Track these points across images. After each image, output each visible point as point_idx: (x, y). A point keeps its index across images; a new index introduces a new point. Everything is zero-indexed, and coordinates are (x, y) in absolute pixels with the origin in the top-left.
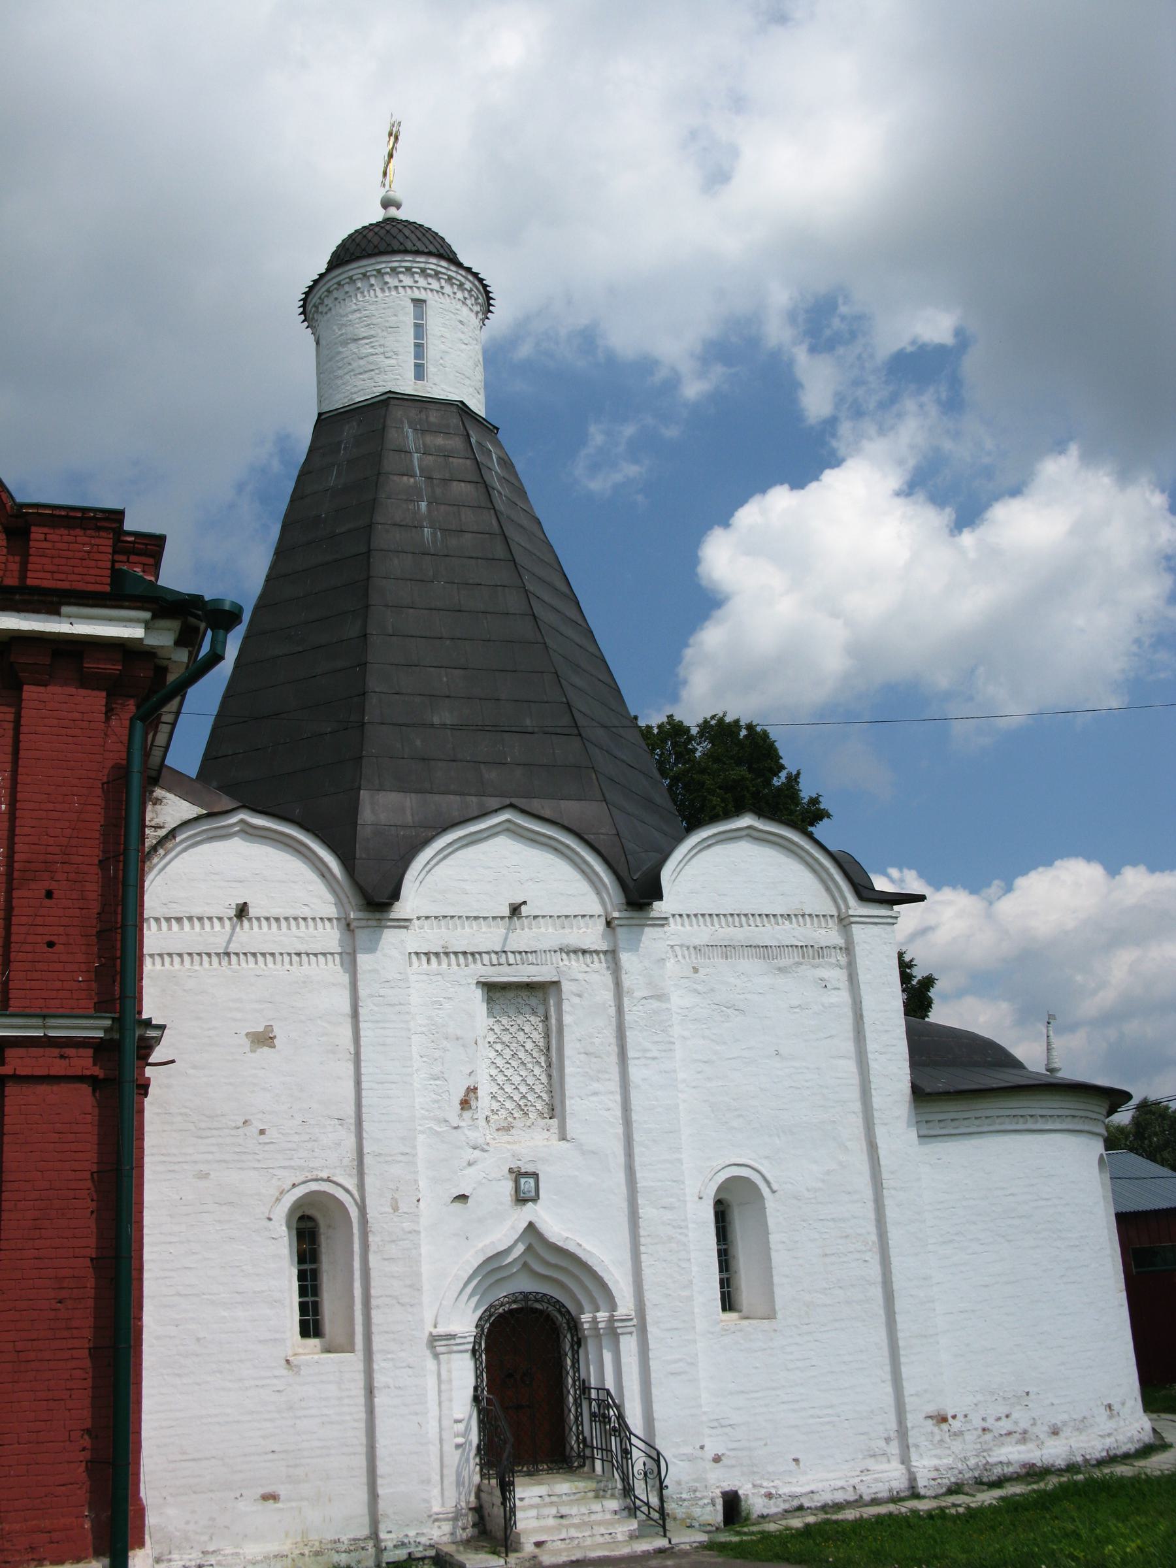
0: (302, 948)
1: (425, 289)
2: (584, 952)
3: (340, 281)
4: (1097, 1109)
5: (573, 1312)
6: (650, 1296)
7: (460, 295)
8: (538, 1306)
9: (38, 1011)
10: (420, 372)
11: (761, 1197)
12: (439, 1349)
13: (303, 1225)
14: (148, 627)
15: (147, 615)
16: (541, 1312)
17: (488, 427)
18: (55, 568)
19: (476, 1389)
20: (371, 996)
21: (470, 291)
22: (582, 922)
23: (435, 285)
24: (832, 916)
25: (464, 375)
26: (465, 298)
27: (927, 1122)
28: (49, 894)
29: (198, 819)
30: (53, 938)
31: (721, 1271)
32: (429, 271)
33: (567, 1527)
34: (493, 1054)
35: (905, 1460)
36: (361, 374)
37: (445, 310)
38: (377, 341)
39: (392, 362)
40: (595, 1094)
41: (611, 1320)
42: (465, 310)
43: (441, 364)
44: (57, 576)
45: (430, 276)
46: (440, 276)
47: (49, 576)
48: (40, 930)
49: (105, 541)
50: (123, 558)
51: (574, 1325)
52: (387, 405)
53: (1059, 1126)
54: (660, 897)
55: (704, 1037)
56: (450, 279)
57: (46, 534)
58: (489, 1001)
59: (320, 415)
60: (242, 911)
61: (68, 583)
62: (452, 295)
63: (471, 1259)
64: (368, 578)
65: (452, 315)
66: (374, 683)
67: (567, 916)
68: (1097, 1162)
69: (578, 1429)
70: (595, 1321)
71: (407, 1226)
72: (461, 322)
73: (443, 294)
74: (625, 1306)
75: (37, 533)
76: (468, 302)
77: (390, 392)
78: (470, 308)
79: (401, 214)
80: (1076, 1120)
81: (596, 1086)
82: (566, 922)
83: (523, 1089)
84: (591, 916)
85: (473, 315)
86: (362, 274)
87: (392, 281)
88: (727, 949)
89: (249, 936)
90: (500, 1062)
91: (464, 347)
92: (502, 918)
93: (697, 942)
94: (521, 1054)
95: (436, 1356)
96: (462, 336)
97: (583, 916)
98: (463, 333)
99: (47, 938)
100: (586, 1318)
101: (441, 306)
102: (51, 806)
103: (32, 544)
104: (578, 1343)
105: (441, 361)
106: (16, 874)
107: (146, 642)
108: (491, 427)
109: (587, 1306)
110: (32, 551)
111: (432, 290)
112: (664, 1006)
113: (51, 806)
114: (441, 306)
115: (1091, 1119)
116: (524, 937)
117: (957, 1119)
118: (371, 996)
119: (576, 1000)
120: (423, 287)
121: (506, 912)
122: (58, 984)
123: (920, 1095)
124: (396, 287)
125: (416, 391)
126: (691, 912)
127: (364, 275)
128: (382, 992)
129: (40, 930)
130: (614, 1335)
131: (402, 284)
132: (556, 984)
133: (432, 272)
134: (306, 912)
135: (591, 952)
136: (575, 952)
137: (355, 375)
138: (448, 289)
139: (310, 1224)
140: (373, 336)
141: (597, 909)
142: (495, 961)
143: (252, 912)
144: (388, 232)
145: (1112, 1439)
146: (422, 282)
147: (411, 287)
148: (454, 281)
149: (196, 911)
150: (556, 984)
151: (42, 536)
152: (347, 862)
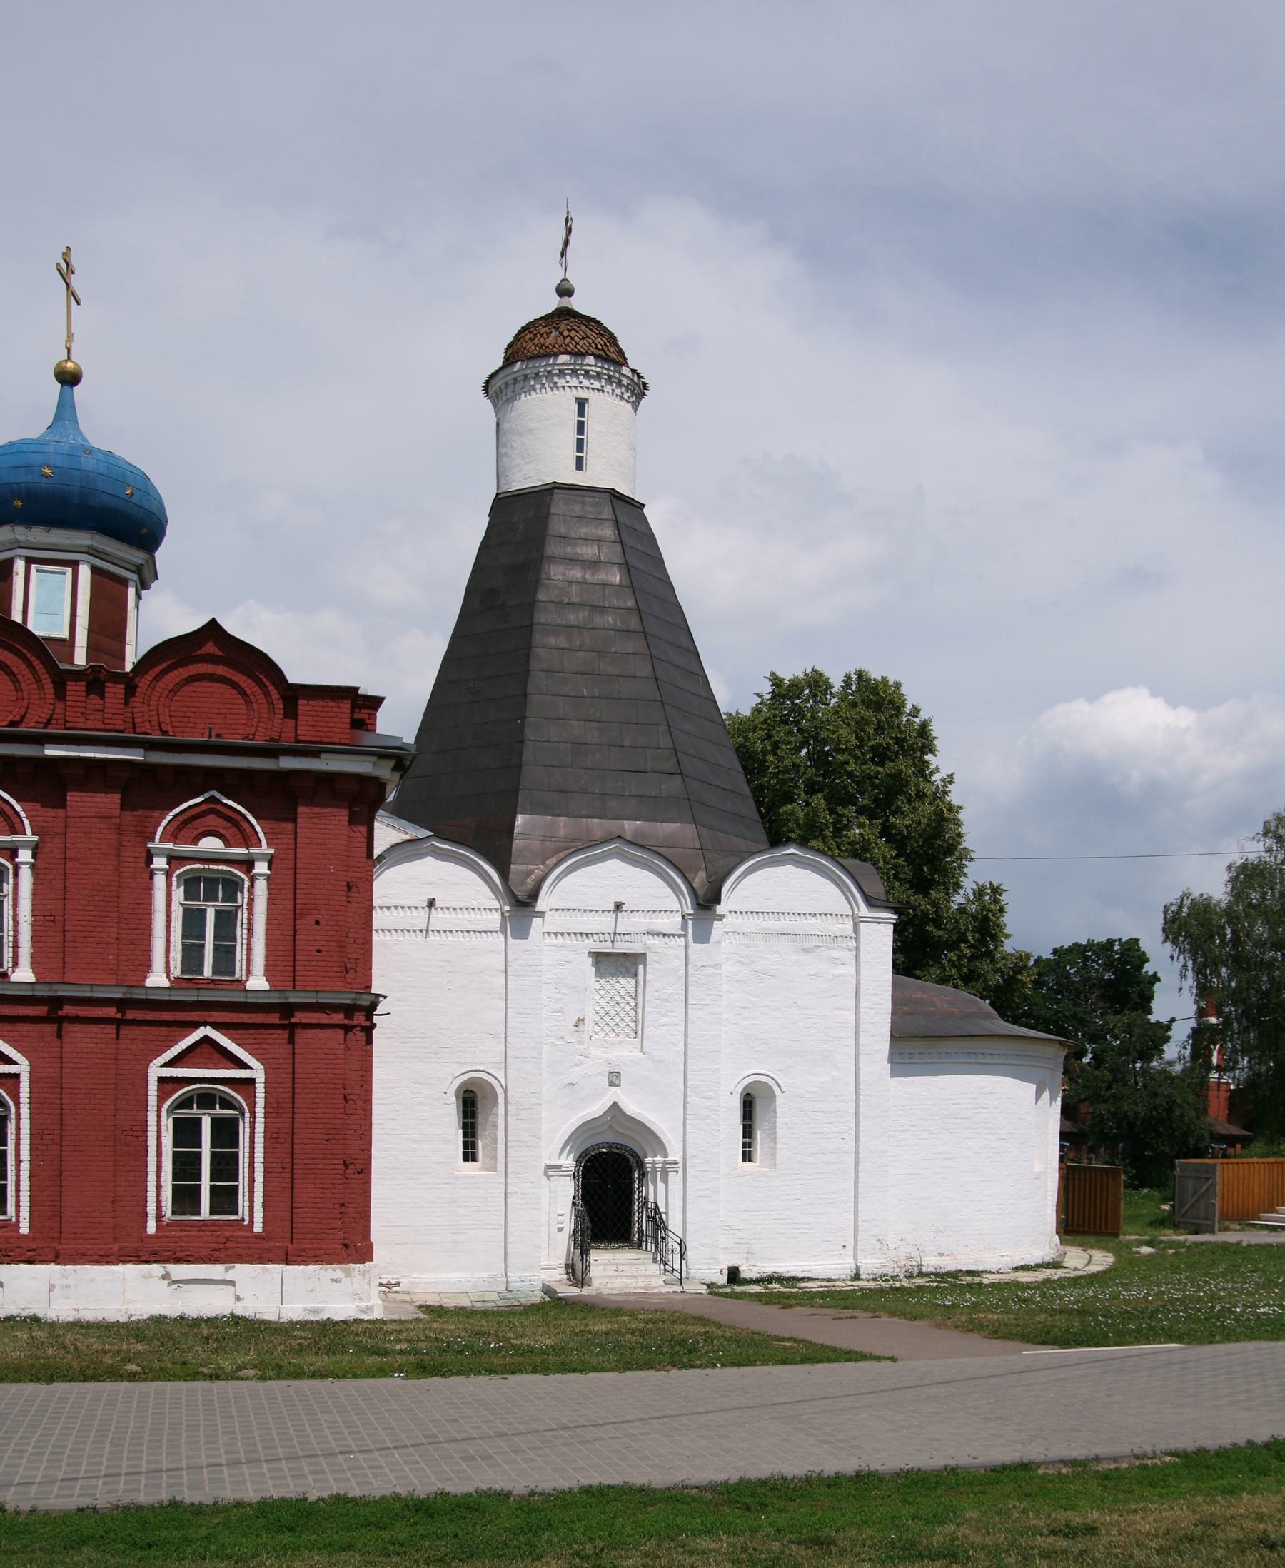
0: (471, 928)
1: (588, 388)
2: (664, 935)
5: (641, 1156)
6: (690, 1152)
7: (618, 391)
8: (618, 1151)
9: (312, 989)
10: (580, 464)
11: (773, 1096)
12: (550, 1173)
13: (467, 1095)
16: (620, 1155)
18: (314, 723)
19: (574, 1198)
20: (516, 960)
22: (665, 915)
23: (597, 385)
24: (847, 916)
28: (317, 923)
30: (321, 948)
31: (744, 1137)
33: (622, 1276)
34: (597, 997)
35: (855, 1258)
41: (665, 1163)
44: (316, 729)
45: (593, 377)
47: (310, 728)
48: (312, 943)
49: (346, 705)
50: (357, 711)
51: (641, 1165)
52: (552, 494)
54: (719, 903)
55: (744, 992)
56: (610, 377)
59: (497, 494)
60: (431, 903)
63: (574, 1122)
64: (530, 648)
66: (529, 733)
67: (654, 911)
70: (654, 1163)
71: (533, 1100)
74: (675, 1155)
76: (626, 396)
81: (666, 1020)
82: (653, 915)
83: (617, 1020)
84: (671, 911)
87: (561, 382)
88: (768, 934)
89: (439, 919)
90: (602, 1002)
92: (609, 911)
93: (746, 930)
94: (618, 998)
95: (548, 1178)
97: (666, 911)
99: (316, 948)
100: (648, 1160)
102: (316, 871)
103: (299, 708)
104: (643, 1175)
106: (298, 911)
109: (649, 1154)
110: (300, 712)
111: (593, 389)
112: (718, 972)
113: (316, 871)
116: (626, 922)
118: (516, 960)
119: (657, 965)
121: (612, 907)
122: (323, 974)
123: (898, 1037)
124: (563, 387)
126: (744, 910)
127: (537, 374)
128: (523, 957)
129: (312, 943)
130: (665, 1173)
132: (644, 955)
134: (474, 904)
135: (669, 935)
136: (658, 934)
139: (471, 1095)
141: (677, 906)
142: (602, 939)
143: (438, 904)
145: (1009, 1259)
146: (586, 383)
147: (576, 387)
149: (400, 903)
150: (644, 955)
152: (504, 875)
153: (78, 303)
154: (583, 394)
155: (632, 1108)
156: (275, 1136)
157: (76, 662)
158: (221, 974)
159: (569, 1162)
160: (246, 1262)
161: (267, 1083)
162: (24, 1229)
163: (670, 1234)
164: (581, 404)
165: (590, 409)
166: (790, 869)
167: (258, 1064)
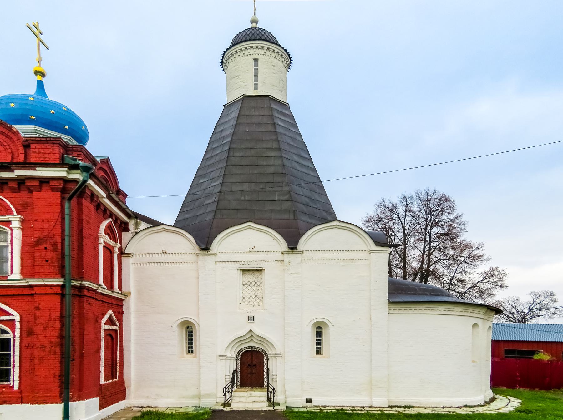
3: (229, 56)
4: (483, 311)
7: (273, 55)
10: (256, 88)
14: (68, 172)
15: (66, 169)
17: (284, 104)
21: (278, 52)
23: (262, 52)
25: (274, 86)
26: (276, 56)
27: (432, 310)
29: (149, 228)
32: (259, 47)
36: (236, 89)
37: (266, 62)
38: (240, 77)
39: (246, 84)
40: (274, 298)
42: (276, 61)
43: (264, 83)
46: (264, 48)
47: (38, 159)
53: (452, 313)
56: (268, 49)
57: (36, 146)
58: (243, 273)
61: (45, 161)
62: (270, 55)
65: (270, 63)
68: (473, 324)
69: (266, 367)
72: (274, 66)
73: (266, 55)
75: (33, 146)
77: (244, 95)
78: (279, 60)
79: (259, 26)
80: (465, 313)
85: (280, 63)
86: (235, 51)
87: (246, 52)
91: (274, 75)
96: (274, 71)
98: (274, 70)
101: (264, 60)
105: (264, 81)
107: (100, 179)
108: (286, 104)
114: (264, 60)
115: (482, 314)
117: (433, 310)
120: (255, 53)
125: (254, 93)
127: (236, 52)
131: (249, 54)
133: (261, 47)
137: (234, 90)
138: (268, 53)
140: (239, 75)
144: (260, 32)
148: (270, 49)
151: (35, 147)
153: (42, 34)
154: (255, 57)
155: (258, 330)
156: (27, 345)
157: (81, 179)
158: (32, 277)
159: (233, 353)
160: (9, 404)
161: (21, 322)
162: (16, 388)
163: (269, 385)
164: (256, 60)
165: (259, 63)
166: (336, 231)
167: (16, 313)
